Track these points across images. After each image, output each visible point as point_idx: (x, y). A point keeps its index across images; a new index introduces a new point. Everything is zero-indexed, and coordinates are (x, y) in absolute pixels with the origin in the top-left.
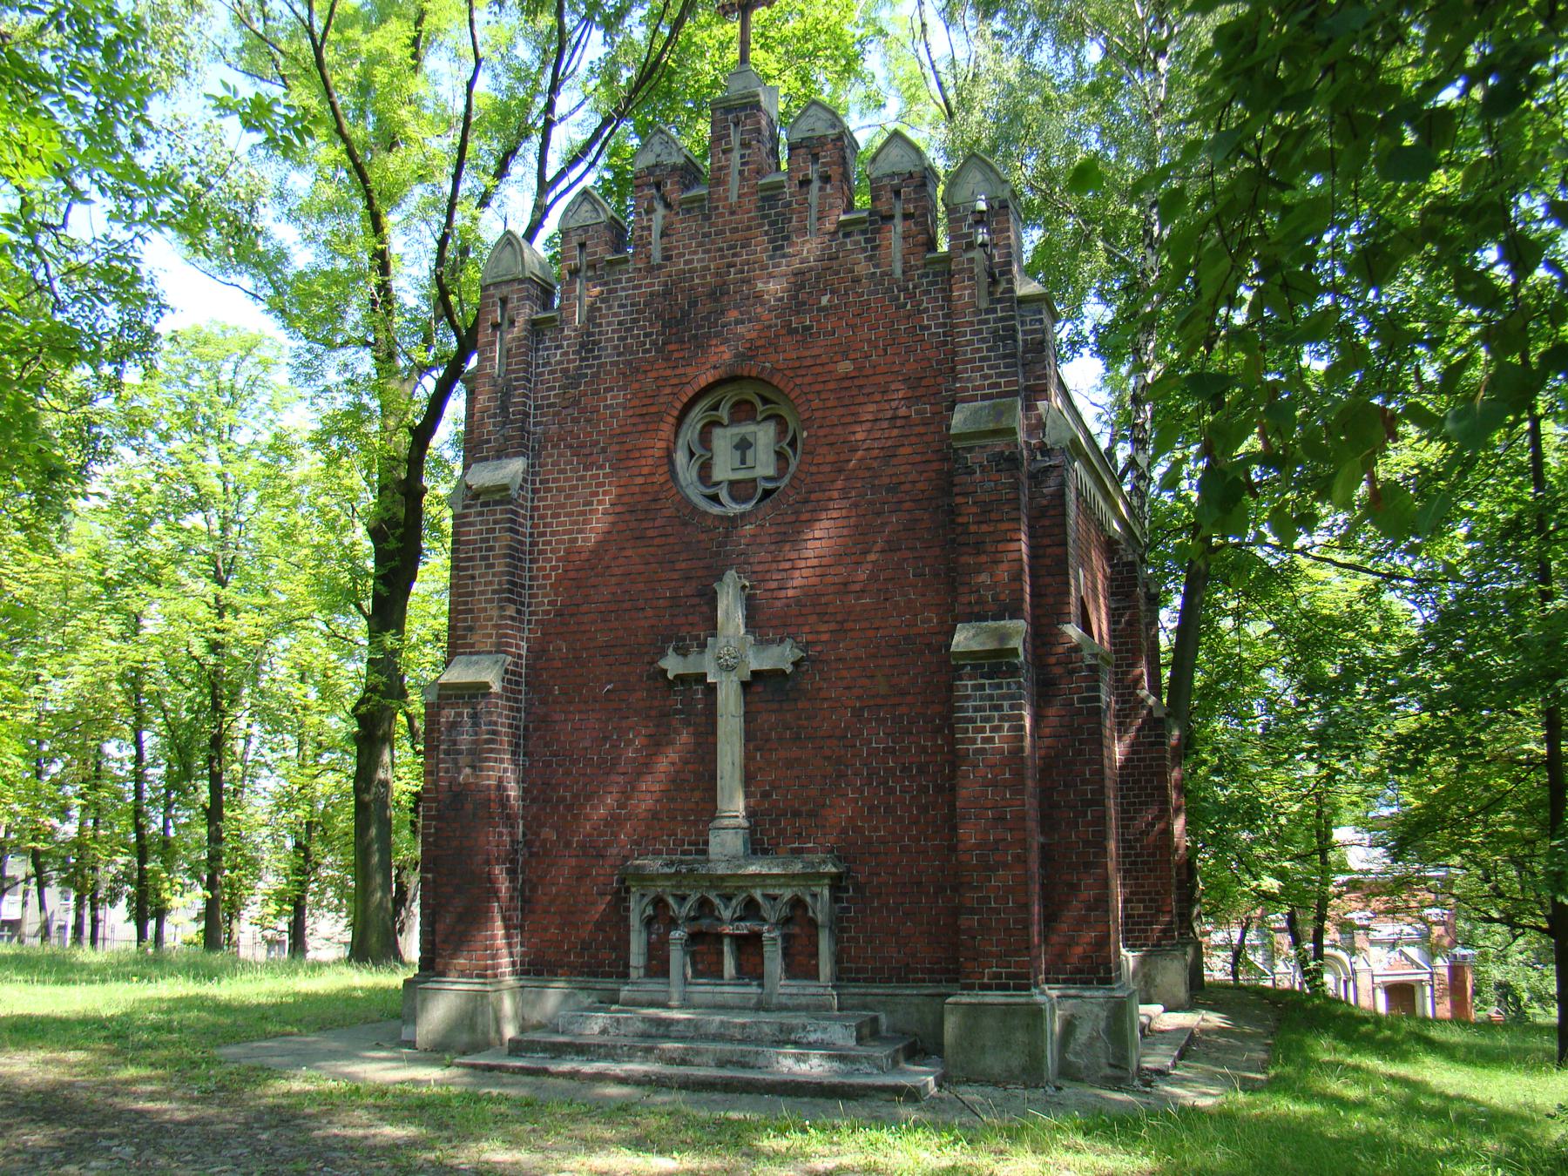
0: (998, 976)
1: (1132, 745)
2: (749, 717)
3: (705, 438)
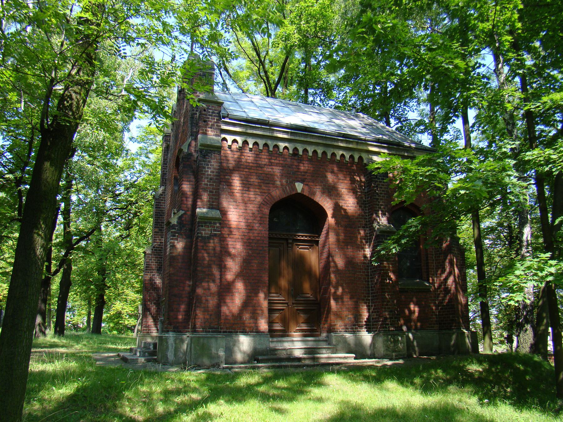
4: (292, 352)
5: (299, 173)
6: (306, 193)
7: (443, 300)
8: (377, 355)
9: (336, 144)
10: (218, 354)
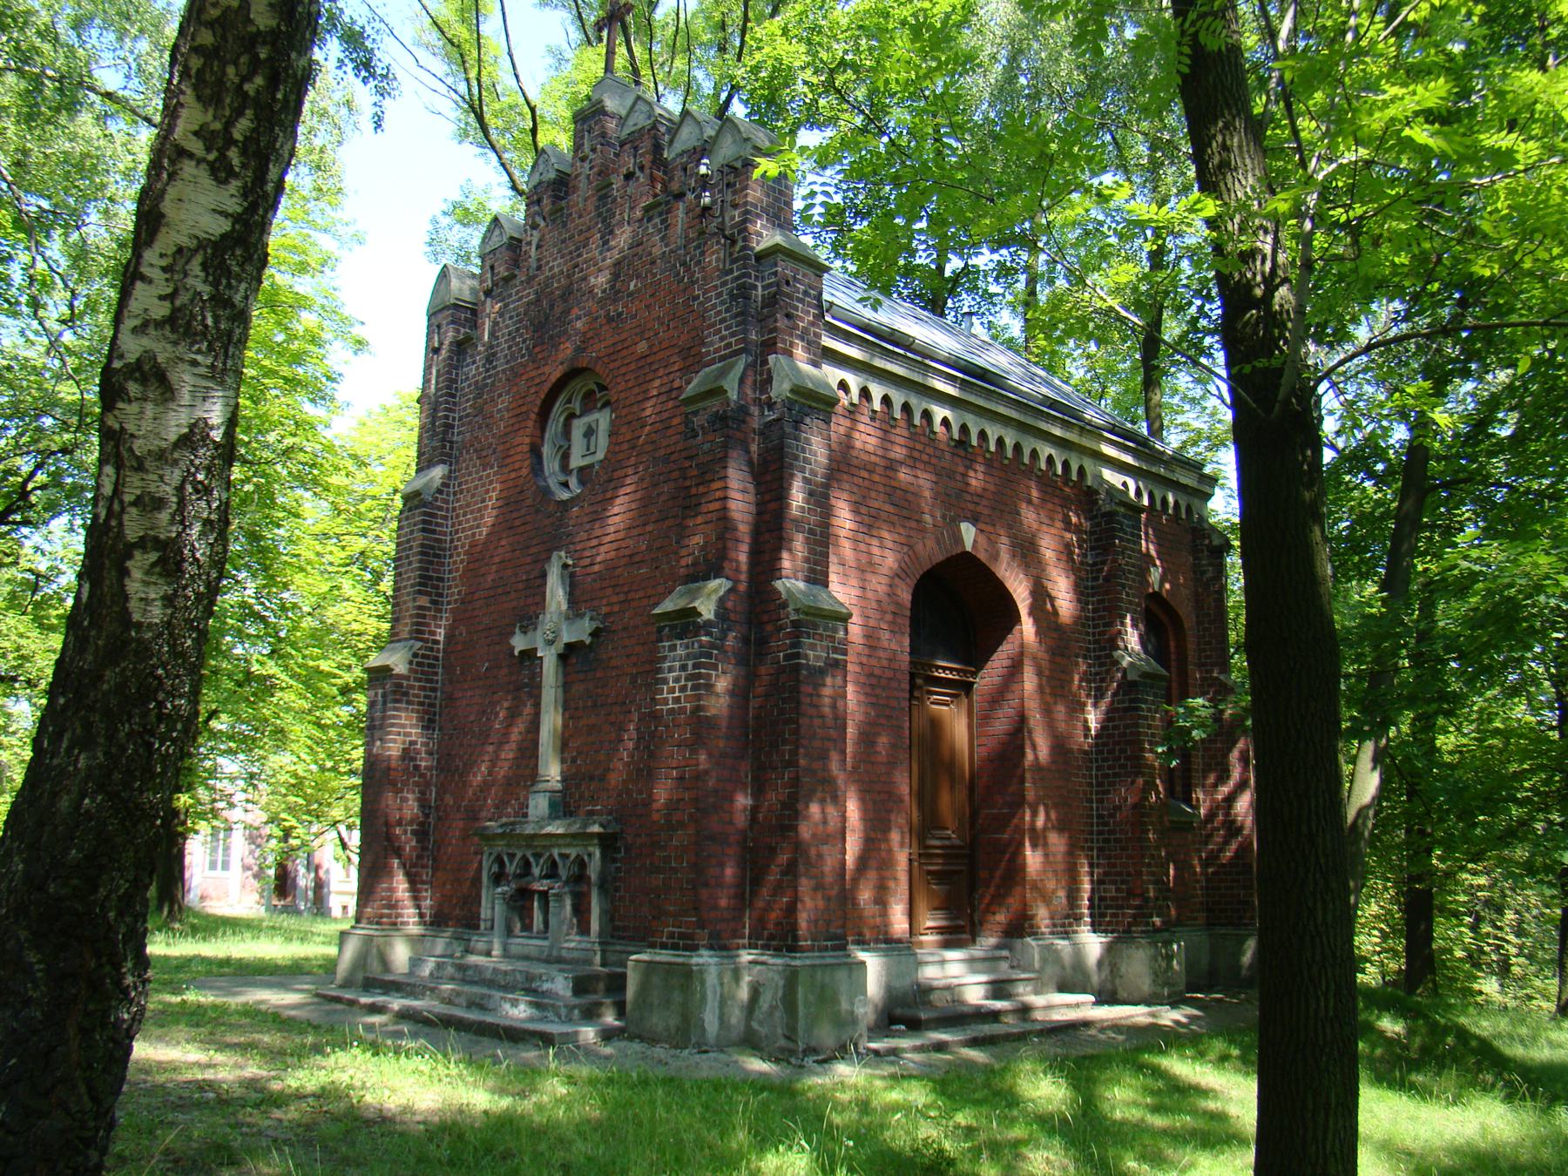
0: (672, 935)
1: (1108, 712)
2: (566, 686)
3: (567, 432)
4: (960, 994)
5: (968, 498)
6: (982, 556)
7: (1221, 850)
8: (1123, 994)
9: (1043, 426)
10: (852, 1012)
